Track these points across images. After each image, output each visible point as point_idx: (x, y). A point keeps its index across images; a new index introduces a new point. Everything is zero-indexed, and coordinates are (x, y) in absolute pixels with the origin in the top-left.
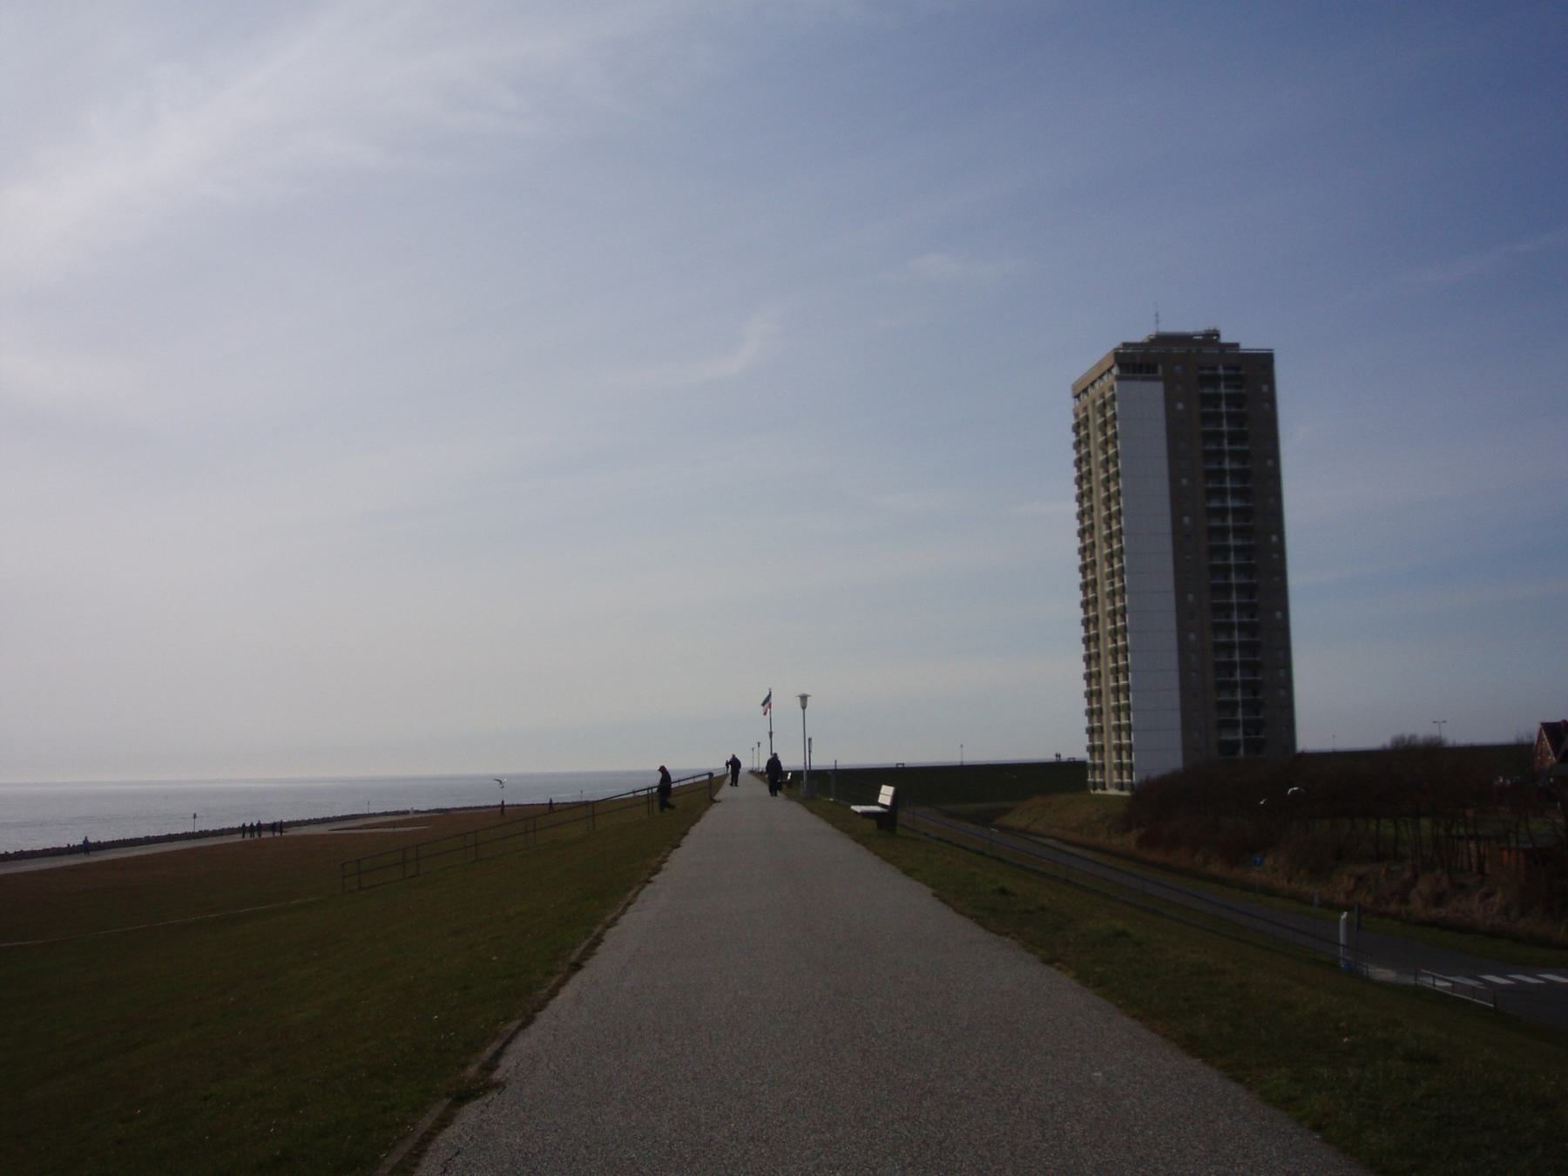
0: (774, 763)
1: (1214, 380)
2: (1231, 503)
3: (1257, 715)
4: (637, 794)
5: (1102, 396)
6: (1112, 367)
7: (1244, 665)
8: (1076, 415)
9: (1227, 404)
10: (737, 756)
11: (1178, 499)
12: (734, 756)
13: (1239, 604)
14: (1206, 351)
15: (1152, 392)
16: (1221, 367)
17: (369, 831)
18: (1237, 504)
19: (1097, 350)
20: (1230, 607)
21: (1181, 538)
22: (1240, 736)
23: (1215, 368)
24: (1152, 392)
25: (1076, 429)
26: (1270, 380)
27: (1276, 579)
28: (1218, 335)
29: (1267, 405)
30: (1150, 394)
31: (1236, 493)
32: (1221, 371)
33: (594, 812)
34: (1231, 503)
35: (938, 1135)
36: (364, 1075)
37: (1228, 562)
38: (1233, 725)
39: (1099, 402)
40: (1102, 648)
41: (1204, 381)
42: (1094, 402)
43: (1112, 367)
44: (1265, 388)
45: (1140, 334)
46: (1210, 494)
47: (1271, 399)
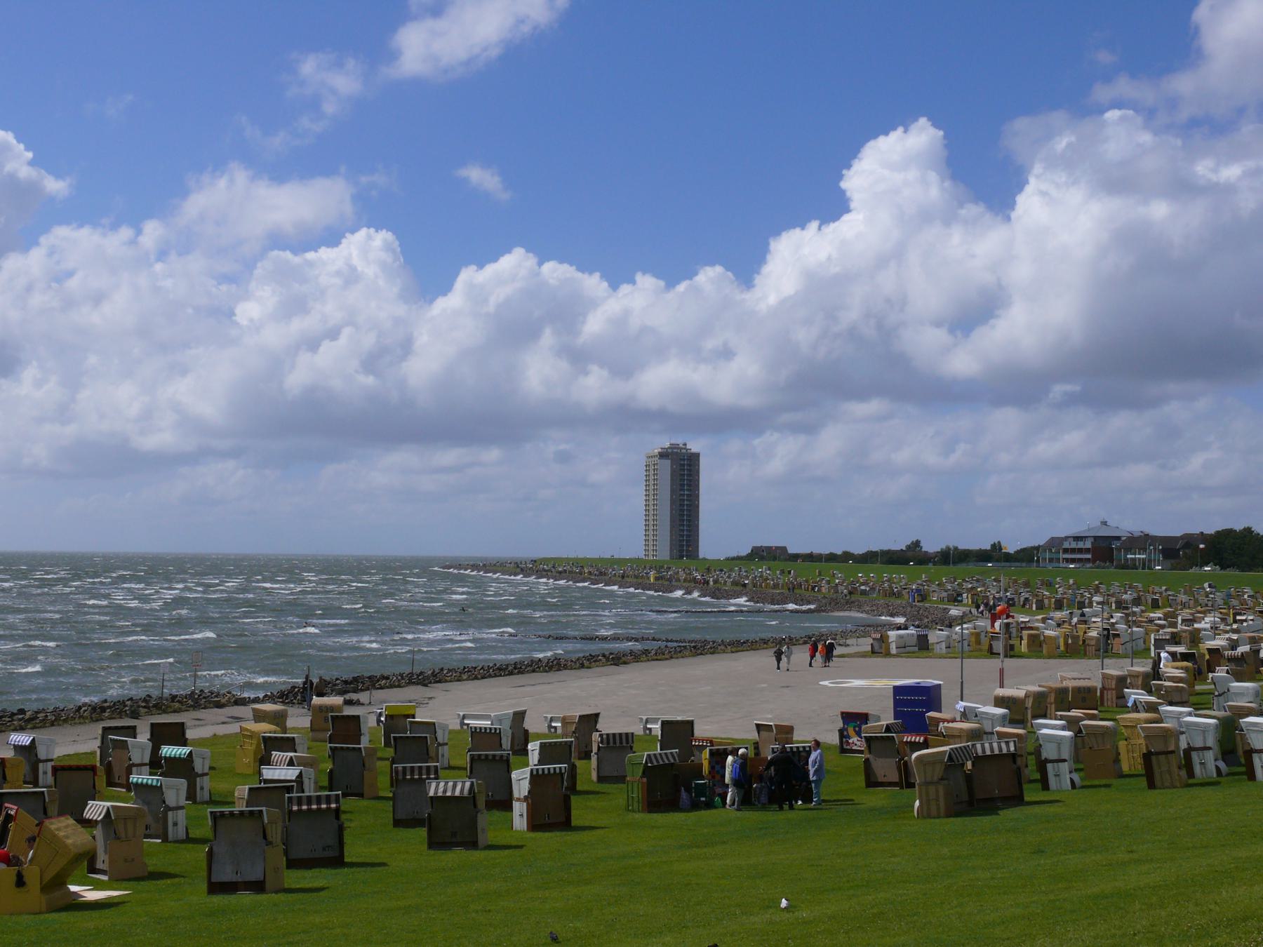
1: (684, 460)
2: (686, 492)
4: (640, 800)
11: (673, 491)
15: (667, 463)
17: (1096, 782)
18: (688, 493)
20: (684, 500)
21: (673, 502)
22: (685, 543)
24: (667, 463)
30: (667, 463)
31: (688, 490)
34: (686, 492)
35: (969, 838)
36: (800, 802)
41: (681, 459)
44: (697, 477)
46: (681, 490)
47: (698, 481)
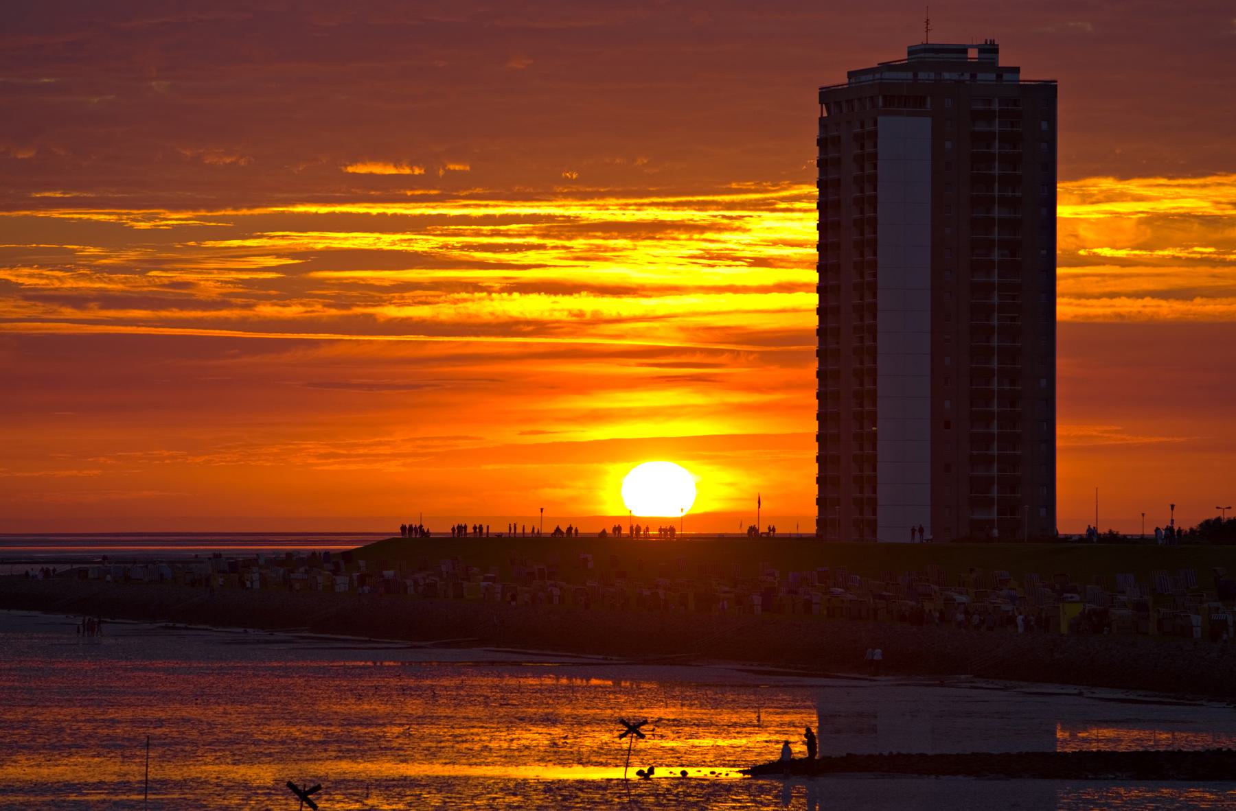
3: (1014, 192)
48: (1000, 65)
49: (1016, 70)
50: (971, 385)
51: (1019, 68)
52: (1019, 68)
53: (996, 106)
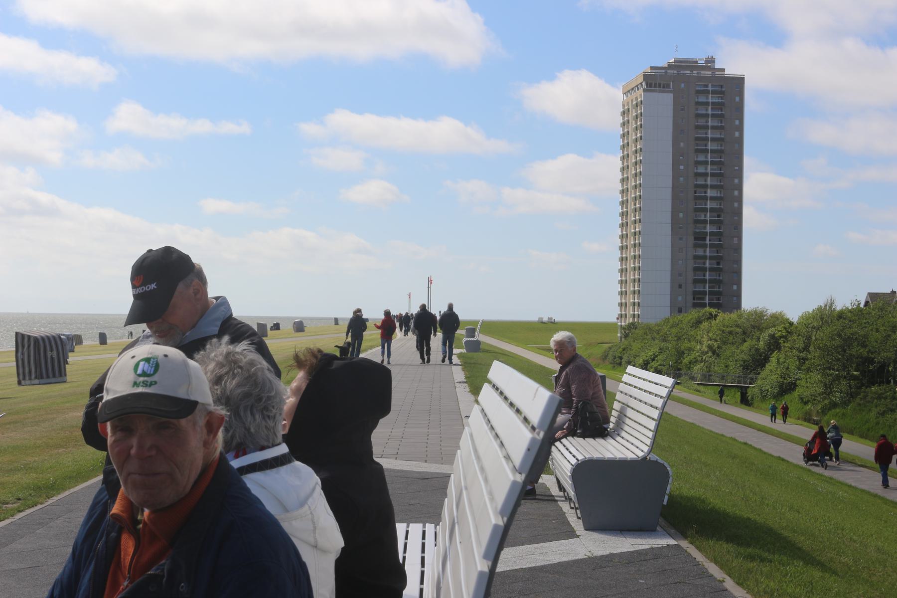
0: (724, 582)
2: (710, 146)
5: (637, 99)
6: (643, 82)
7: (711, 246)
8: (624, 106)
9: (712, 108)
10: (456, 310)
12: (451, 307)
13: (711, 209)
14: (704, 73)
16: (710, 85)
19: (636, 72)
23: (707, 86)
24: (667, 99)
25: (623, 113)
26: (741, 93)
27: (735, 266)
28: (714, 62)
29: (736, 145)
32: (710, 88)
33: (571, 464)
37: (707, 183)
38: (704, 281)
39: (634, 103)
40: (628, 243)
42: (632, 100)
43: (643, 82)
45: (664, 59)
48: (716, 67)
49: (723, 70)
50: (694, 299)
51: (724, 69)
52: (724, 69)
53: (710, 88)
